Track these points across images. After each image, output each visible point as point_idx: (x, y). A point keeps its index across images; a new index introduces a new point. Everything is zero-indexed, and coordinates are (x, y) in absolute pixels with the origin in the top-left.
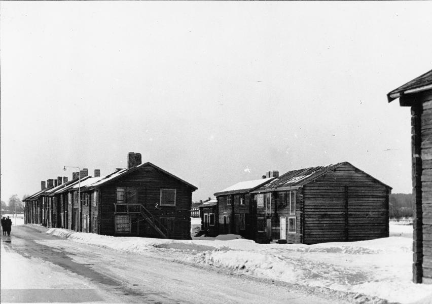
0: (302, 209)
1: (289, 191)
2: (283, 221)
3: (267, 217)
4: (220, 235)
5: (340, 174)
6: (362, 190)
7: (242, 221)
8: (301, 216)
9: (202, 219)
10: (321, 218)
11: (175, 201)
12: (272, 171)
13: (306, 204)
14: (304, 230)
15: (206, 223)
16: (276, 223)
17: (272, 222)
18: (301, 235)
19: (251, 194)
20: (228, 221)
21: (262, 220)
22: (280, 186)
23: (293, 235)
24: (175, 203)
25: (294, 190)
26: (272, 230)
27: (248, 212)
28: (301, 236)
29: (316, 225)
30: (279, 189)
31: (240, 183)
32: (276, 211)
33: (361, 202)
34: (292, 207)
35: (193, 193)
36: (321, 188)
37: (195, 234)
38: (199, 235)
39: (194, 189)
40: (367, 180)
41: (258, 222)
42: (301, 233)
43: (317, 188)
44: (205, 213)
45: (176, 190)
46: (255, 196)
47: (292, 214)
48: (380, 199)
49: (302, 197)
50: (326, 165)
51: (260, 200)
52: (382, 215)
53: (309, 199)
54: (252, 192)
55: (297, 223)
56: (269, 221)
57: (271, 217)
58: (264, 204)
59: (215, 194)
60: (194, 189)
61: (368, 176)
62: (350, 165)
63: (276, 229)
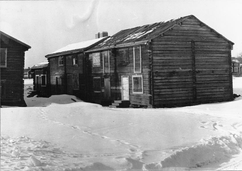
0: (151, 66)
1: (132, 47)
2: (125, 80)
3: (105, 76)
4: (53, 96)
5: (186, 28)
6: (207, 46)
7: (76, 81)
8: (150, 75)
9: (34, 81)
10: (170, 76)
11: (6, 61)
12: (101, 32)
13: (154, 61)
14: (153, 90)
15: (38, 84)
16: (117, 82)
17: (111, 82)
18: (149, 95)
19: (85, 53)
20: (60, 82)
21: (99, 79)
22: (118, 43)
23: (138, 96)
24: (6, 64)
25: (139, 46)
26: (111, 89)
27: (81, 72)
28: (150, 97)
29: (165, 83)
30: (118, 46)
31: (69, 45)
32: (115, 70)
33: (207, 57)
34: (137, 65)
35: (26, 52)
36: (169, 43)
37: (28, 95)
38: (31, 95)
39: (27, 48)
40: (212, 35)
41: (94, 81)
42: (150, 93)
43: (164, 43)
44: (38, 74)
45: (7, 49)
46: (90, 56)
47: (137, 72)
48: (224, 55)
49: (150, 53)
50: (166, 20)
51: (96, 59)
52: (226, 71)
53: (157, 55)
54: (87, 51)
55: (144, 83)
56: (107, 81)
57: (109, 76)
58: (101, 63)
59: (46, 56)
60: (27, 48)
61: (212, 30)
62: (195, 18)
63: (116, 89)
